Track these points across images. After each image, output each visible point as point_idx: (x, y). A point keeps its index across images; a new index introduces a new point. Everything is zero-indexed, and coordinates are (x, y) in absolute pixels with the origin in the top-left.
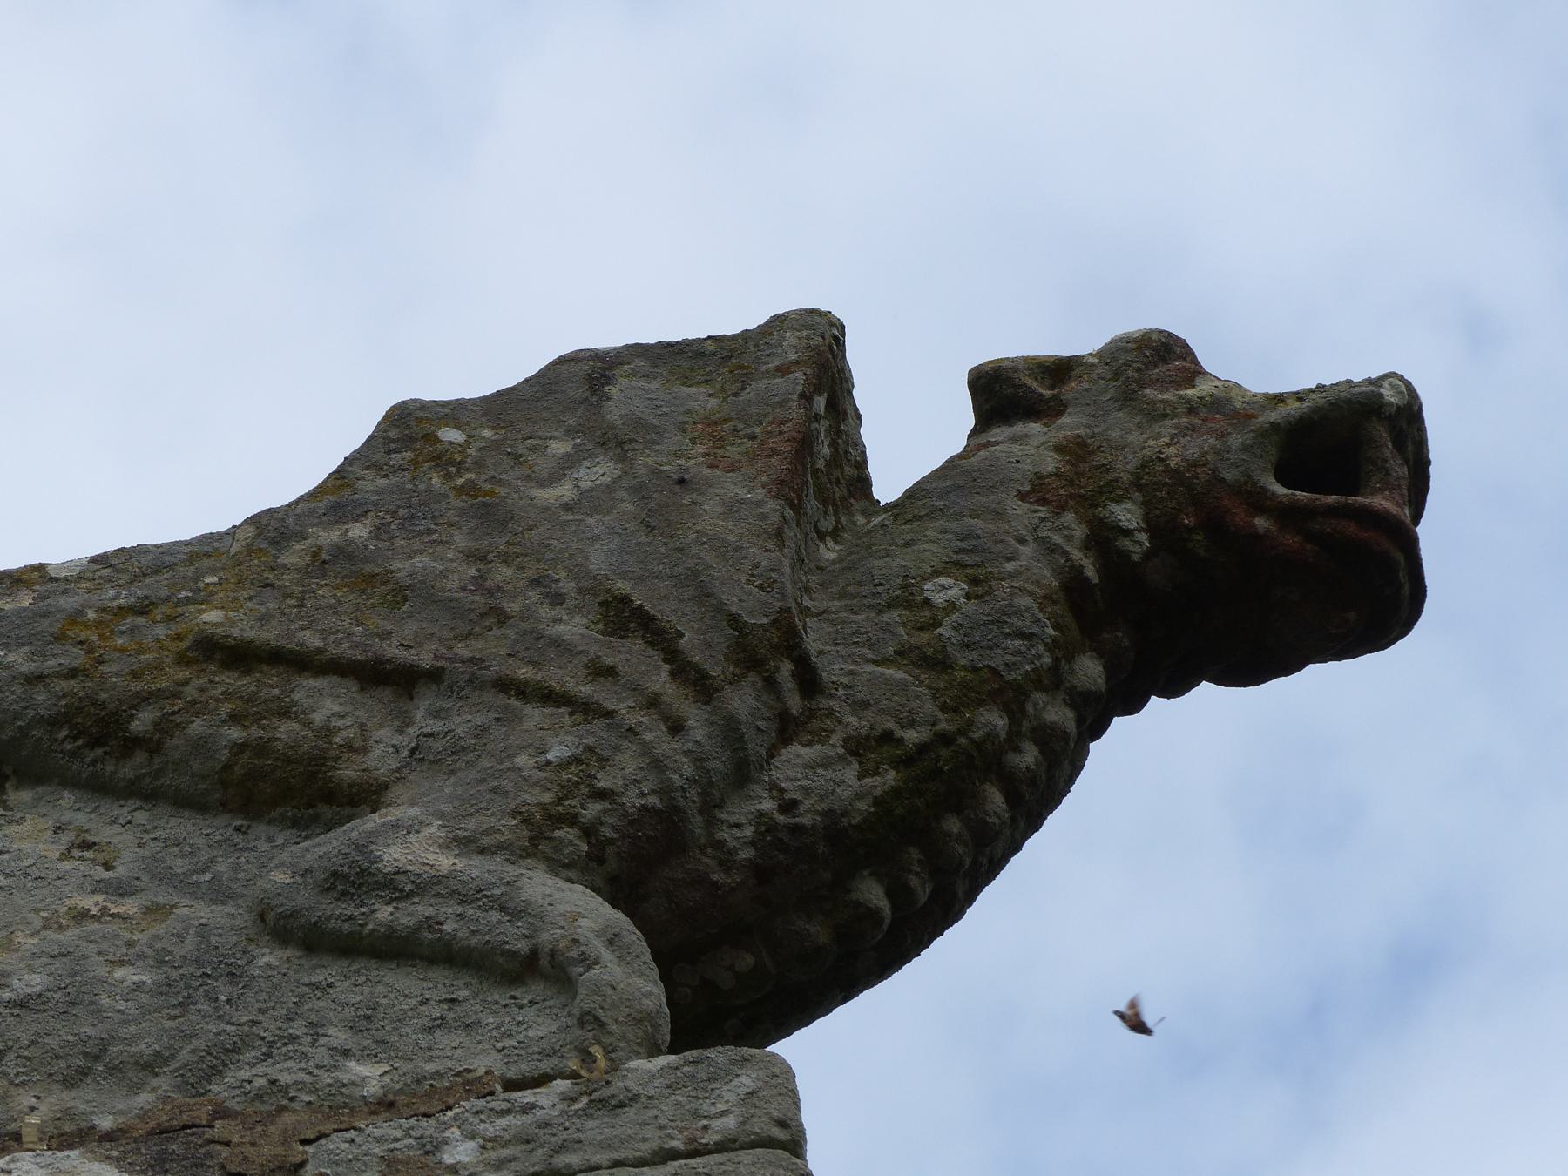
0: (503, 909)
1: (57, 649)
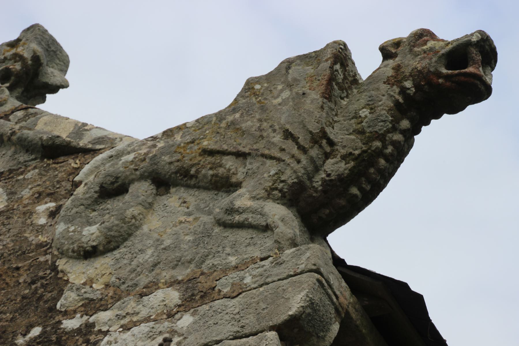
0: (261, 214)
1: (175, 155)
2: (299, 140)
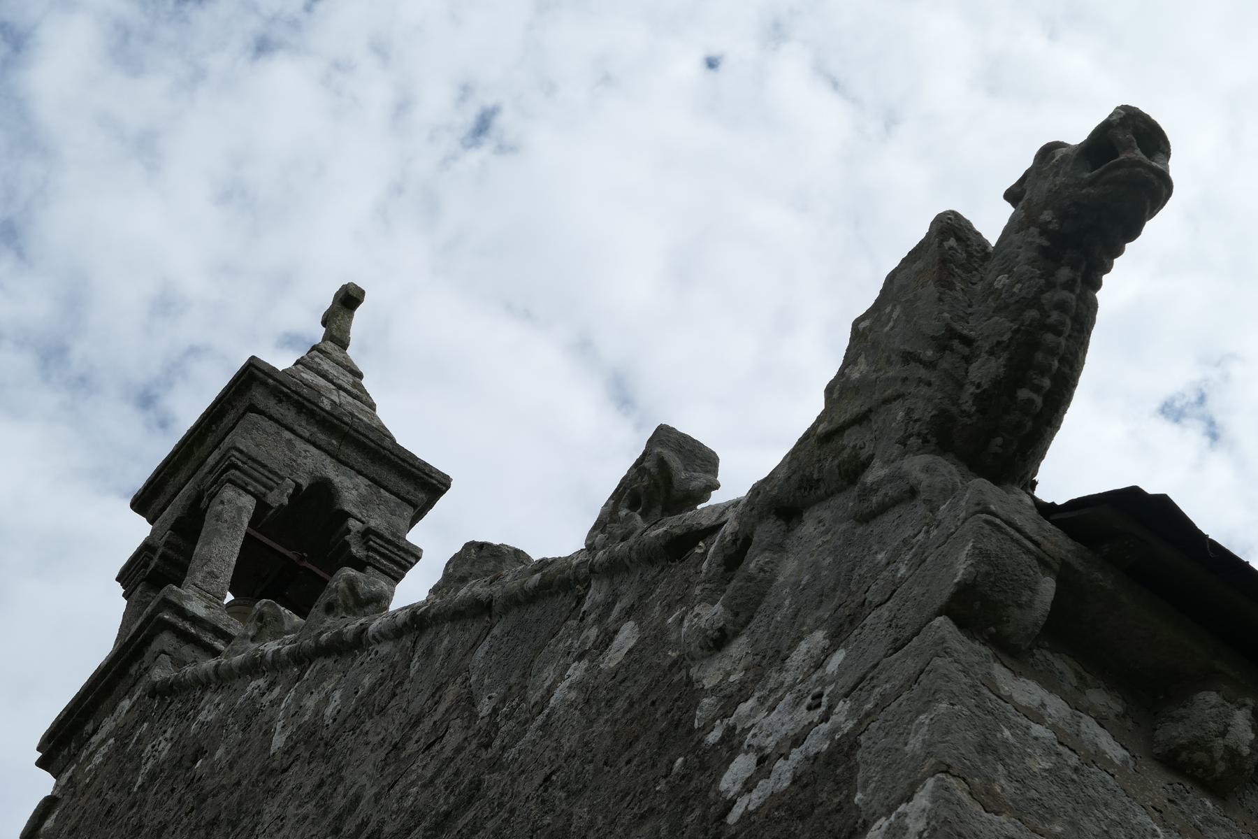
2: (921, 356)
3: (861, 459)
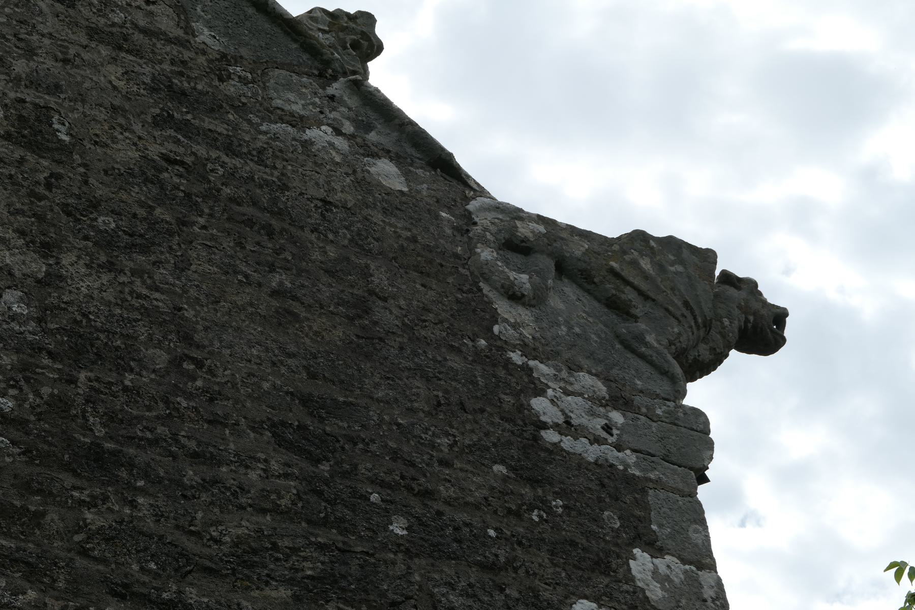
3: (631, 311)
